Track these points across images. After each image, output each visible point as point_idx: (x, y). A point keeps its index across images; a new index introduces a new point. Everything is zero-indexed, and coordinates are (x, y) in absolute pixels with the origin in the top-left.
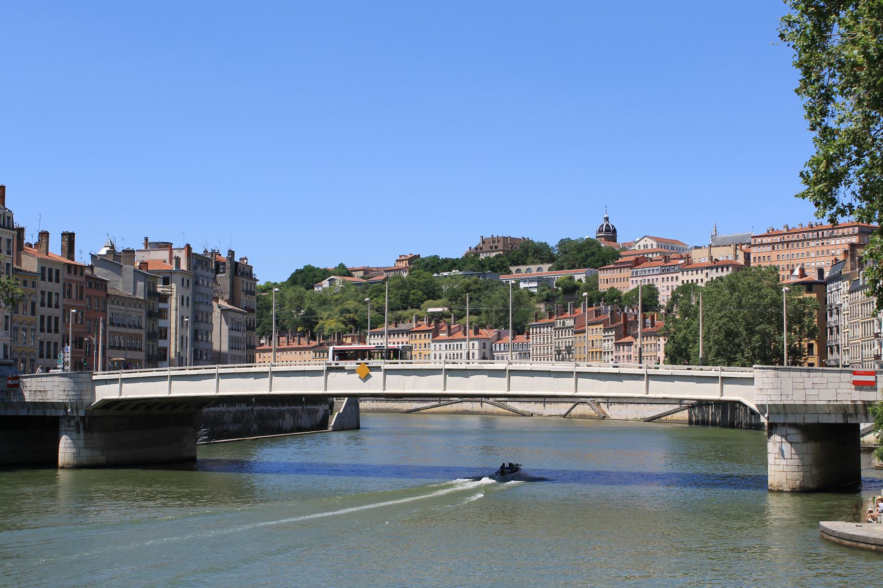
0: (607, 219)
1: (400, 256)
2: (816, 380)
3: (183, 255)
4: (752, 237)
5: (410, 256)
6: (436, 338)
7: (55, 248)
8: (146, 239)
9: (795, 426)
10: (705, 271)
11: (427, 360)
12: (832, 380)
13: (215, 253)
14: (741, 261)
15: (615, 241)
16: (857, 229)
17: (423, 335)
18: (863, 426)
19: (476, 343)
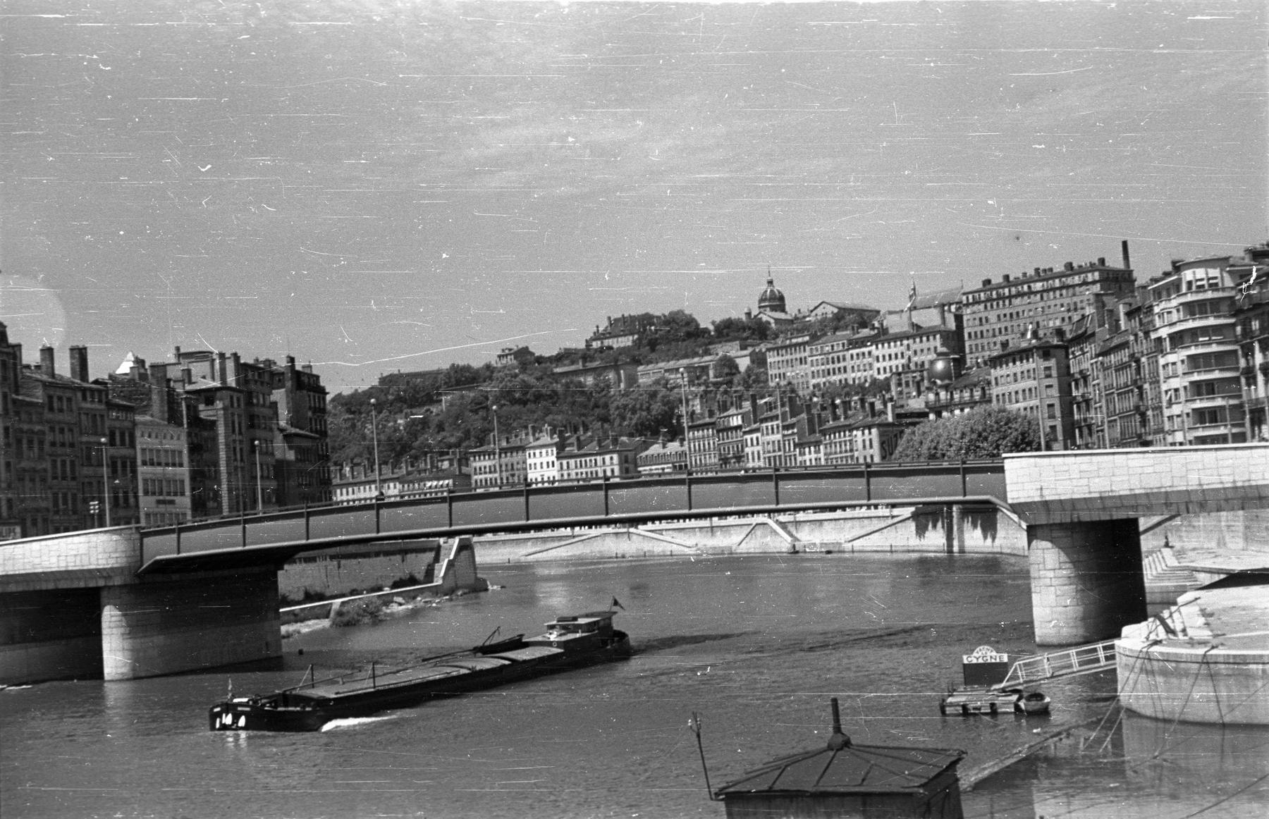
0: (770, 282)
1: (503, 350)
2: (1084, 467)
3: (230, 365)
4: (964, 294)
5: (515, 349)
6: (562, 455)
7: (63, 367)
8: (178, 349)
9: (1061, 526)
10: (905, 342)
11: (328, 502)
12: (1104, 465)
13: (269, 363)
14: (952, 325)
15: (783, 310)
16: (1097, 274)
17: (544, 451)
18: (1143, 523)
19: (615, 456)
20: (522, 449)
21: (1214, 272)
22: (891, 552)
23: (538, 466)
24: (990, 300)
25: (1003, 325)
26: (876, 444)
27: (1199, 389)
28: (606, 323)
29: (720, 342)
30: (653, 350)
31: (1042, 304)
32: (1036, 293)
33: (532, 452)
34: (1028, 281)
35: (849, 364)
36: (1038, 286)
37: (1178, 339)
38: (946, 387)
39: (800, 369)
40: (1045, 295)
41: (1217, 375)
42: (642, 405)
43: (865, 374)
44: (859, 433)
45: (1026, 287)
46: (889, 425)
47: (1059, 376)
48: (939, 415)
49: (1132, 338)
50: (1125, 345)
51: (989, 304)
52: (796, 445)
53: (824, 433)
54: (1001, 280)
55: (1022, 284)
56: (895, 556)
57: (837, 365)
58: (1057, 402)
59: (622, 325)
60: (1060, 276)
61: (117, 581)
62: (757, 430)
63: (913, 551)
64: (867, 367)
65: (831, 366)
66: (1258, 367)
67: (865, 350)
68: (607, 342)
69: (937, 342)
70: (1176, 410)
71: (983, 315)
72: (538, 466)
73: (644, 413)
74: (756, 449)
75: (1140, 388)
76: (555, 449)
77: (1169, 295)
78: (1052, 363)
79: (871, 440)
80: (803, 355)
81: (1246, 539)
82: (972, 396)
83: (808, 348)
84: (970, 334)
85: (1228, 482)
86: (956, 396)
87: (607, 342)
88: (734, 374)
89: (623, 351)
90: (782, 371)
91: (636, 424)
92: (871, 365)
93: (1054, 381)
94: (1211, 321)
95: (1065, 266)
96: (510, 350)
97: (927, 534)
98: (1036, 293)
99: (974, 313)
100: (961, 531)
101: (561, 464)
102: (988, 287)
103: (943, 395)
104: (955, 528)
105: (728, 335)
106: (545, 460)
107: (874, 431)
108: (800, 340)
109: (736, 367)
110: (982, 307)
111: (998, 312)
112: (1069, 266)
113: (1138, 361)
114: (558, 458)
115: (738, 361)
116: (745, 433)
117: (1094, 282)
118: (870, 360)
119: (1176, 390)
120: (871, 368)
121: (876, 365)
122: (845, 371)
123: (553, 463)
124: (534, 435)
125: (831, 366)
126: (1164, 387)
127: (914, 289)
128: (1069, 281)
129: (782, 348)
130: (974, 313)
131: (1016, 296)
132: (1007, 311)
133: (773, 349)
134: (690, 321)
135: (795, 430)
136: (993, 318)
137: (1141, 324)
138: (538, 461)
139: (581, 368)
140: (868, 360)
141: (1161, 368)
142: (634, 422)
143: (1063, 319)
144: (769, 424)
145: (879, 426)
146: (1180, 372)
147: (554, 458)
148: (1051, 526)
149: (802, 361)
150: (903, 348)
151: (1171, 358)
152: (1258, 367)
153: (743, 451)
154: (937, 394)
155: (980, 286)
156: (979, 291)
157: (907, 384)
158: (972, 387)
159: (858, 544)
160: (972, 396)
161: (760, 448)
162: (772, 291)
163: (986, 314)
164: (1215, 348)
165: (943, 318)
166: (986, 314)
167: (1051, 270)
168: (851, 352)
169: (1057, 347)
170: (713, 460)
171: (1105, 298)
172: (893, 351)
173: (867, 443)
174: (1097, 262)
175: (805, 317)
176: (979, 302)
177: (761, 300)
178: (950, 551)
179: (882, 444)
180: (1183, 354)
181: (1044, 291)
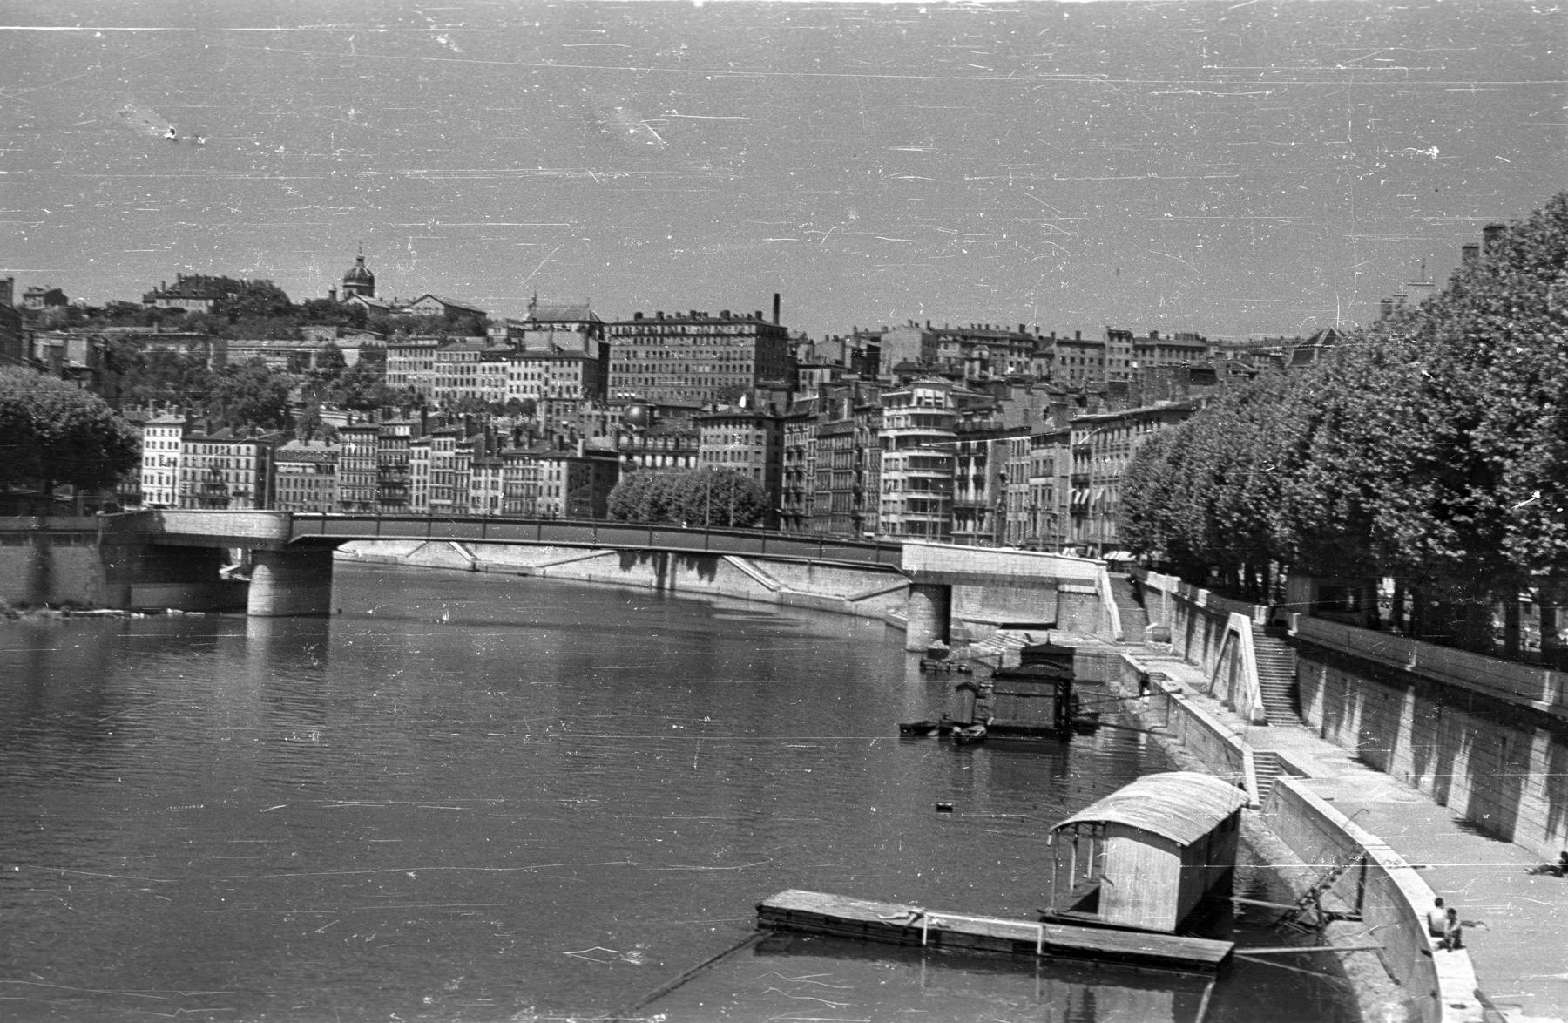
0: (361, 260)
1: (30, 289)
5: (47, 290)
6: (187, 437)
9: (933, 586)
14: (595, 353)
17: (167, 430)
19: (253, 447)
20: (141, 424)
21: (940, 394)
22: (589, 581)
23: (158, 445)
24: (641, 334)
25: (650, 363)
26: (564, 476)
27: (916, 483)
28: (175, 281)
29: (314, 325)
30: (233, 321)
31: (694, 348)
32: (688, 336)
33: (151, 429)
34: (683, 321)
35: (479, 376)
36: (693, 329)
37: (902, 442)
38: (641, 434)
39: (424, 374)
40: (698, 340)
41: (932, 475)
42: (249, 389)
43: (496, 390)
44: (546, 464)
45: (679, 328)
46: (578, 460)
47: (769, 444)
48: (630, 456)
49: (857, 430)
50: (850, 434)
51: (639, 339)
52: (470, 465)
53: (506, 457)
54: (653, 316)
55: (676, 324)
56: (593, 585)
57: (465, 376)
58: (762, 466)
59: (192, 286)
60: (716, 323)
61: (271, 548)
62: (427, 444)
63: (614, 583)
64: (499, 383)
65: (458, 376)
66: (971, 476)
67: (499, 365)
68: (176, 303)
69: (578, 369)
70: (893, 496)
71: (632, 349)
72: (158, 445)
73: (252, 399)
74: (422, 462)
75: (860, 473)
76: (180, 430)
77: (899, 404)
78: (763, 433)
79: (558, 472)
80: (428, 359)
81: (983, 605)
82: (665, 445)
83: (435, 353)
84: (614, 366)
85: (1027, 572)
86: (650, 443)
87: (176, 303)
88: (341, 366)
89: (198, 316)
90: (402, 373)
91: (243, 410)
92: (503, 382)
93: (763, 449)
94: (933, 432)
95: (722, 314)
96: (39, 290)
97: (633, 568)
98: (688, 336)
99: (622, 345)
100: (674, 570)
101: (186, 447)
102: (640, 321)
103: (637, 440)
104: (669, 567)
105: (323, 318)
106: (166, 440)
107: (564, 464)
108: (427, 343)
109: (342, 357)
110: (631, 341)
111: (648, 348)
112: (726, 314)
113: (860, 451)
114: (183, 440)
115: (345, 351)
116: (414, 445)
117: (750, 335)
118: (504, 376)
119: (896, 481)
120: (503, 385)
121: (509, 382)
122: (474, 384)
123: (176, 444)
124: (155, 411)
125: (458, 376)
126: (884, 476)
127: (535, 299)
128: (725, 330)
129: (405, 348)
130: (622, 345)
131: (668, 336)
132: (658, 349)
133: (395, 348)
134: (278, 295)
135: (472, 450)
136: (642, 354)
137: (869, 420)
138: (158, 439)
139: (156, 333)
140: (500, 376)
141: (883, 462)
142: (240, 407)
143: (714, 367)
144: (442, 440)
145: (570, 460)
146: (901, 467)
147: (178, 439)
148: (927, 585)
149: (428, 366)
150: (541, 370)
151: (895, 455)
152: (971, 476)
153: (407, 462)
154: (631, 438)
155: (631, 318)
156: (629, 324)
157: (558, 411)
158: (667, 436)
159: (550, 570)
160: (665, 445)
161: (428, 462)
162: (362, 270)
163: (634, 348)
164: (933, 454)
165: (587, 345)
166: (634, 348)
167: (706, 314)
168: (483, 364)
169: (769, 419)
170: (370, 466)
171: (828, 389)
172: (530, 370)
173: (555, 474)
174: (754, 316)
175: (402, 307)
176: (629, 336)
177: (347, 279)
178: (660, 587)
179: (570, 477)
180: (907, 454)
181: (698, 335)
